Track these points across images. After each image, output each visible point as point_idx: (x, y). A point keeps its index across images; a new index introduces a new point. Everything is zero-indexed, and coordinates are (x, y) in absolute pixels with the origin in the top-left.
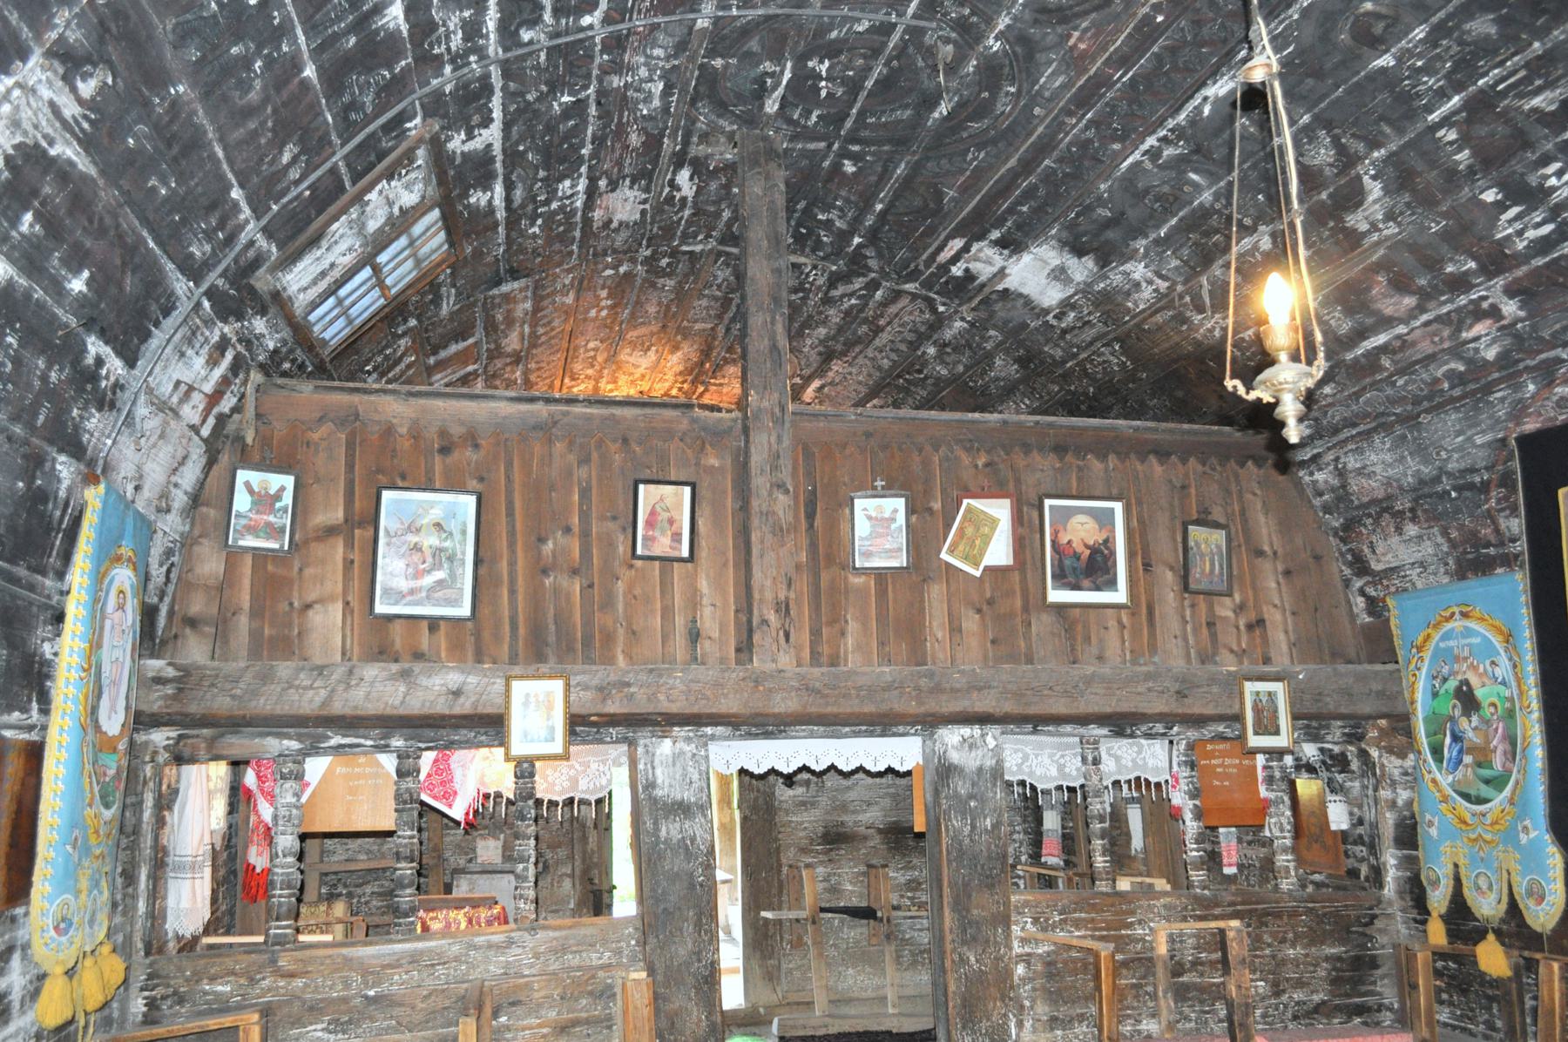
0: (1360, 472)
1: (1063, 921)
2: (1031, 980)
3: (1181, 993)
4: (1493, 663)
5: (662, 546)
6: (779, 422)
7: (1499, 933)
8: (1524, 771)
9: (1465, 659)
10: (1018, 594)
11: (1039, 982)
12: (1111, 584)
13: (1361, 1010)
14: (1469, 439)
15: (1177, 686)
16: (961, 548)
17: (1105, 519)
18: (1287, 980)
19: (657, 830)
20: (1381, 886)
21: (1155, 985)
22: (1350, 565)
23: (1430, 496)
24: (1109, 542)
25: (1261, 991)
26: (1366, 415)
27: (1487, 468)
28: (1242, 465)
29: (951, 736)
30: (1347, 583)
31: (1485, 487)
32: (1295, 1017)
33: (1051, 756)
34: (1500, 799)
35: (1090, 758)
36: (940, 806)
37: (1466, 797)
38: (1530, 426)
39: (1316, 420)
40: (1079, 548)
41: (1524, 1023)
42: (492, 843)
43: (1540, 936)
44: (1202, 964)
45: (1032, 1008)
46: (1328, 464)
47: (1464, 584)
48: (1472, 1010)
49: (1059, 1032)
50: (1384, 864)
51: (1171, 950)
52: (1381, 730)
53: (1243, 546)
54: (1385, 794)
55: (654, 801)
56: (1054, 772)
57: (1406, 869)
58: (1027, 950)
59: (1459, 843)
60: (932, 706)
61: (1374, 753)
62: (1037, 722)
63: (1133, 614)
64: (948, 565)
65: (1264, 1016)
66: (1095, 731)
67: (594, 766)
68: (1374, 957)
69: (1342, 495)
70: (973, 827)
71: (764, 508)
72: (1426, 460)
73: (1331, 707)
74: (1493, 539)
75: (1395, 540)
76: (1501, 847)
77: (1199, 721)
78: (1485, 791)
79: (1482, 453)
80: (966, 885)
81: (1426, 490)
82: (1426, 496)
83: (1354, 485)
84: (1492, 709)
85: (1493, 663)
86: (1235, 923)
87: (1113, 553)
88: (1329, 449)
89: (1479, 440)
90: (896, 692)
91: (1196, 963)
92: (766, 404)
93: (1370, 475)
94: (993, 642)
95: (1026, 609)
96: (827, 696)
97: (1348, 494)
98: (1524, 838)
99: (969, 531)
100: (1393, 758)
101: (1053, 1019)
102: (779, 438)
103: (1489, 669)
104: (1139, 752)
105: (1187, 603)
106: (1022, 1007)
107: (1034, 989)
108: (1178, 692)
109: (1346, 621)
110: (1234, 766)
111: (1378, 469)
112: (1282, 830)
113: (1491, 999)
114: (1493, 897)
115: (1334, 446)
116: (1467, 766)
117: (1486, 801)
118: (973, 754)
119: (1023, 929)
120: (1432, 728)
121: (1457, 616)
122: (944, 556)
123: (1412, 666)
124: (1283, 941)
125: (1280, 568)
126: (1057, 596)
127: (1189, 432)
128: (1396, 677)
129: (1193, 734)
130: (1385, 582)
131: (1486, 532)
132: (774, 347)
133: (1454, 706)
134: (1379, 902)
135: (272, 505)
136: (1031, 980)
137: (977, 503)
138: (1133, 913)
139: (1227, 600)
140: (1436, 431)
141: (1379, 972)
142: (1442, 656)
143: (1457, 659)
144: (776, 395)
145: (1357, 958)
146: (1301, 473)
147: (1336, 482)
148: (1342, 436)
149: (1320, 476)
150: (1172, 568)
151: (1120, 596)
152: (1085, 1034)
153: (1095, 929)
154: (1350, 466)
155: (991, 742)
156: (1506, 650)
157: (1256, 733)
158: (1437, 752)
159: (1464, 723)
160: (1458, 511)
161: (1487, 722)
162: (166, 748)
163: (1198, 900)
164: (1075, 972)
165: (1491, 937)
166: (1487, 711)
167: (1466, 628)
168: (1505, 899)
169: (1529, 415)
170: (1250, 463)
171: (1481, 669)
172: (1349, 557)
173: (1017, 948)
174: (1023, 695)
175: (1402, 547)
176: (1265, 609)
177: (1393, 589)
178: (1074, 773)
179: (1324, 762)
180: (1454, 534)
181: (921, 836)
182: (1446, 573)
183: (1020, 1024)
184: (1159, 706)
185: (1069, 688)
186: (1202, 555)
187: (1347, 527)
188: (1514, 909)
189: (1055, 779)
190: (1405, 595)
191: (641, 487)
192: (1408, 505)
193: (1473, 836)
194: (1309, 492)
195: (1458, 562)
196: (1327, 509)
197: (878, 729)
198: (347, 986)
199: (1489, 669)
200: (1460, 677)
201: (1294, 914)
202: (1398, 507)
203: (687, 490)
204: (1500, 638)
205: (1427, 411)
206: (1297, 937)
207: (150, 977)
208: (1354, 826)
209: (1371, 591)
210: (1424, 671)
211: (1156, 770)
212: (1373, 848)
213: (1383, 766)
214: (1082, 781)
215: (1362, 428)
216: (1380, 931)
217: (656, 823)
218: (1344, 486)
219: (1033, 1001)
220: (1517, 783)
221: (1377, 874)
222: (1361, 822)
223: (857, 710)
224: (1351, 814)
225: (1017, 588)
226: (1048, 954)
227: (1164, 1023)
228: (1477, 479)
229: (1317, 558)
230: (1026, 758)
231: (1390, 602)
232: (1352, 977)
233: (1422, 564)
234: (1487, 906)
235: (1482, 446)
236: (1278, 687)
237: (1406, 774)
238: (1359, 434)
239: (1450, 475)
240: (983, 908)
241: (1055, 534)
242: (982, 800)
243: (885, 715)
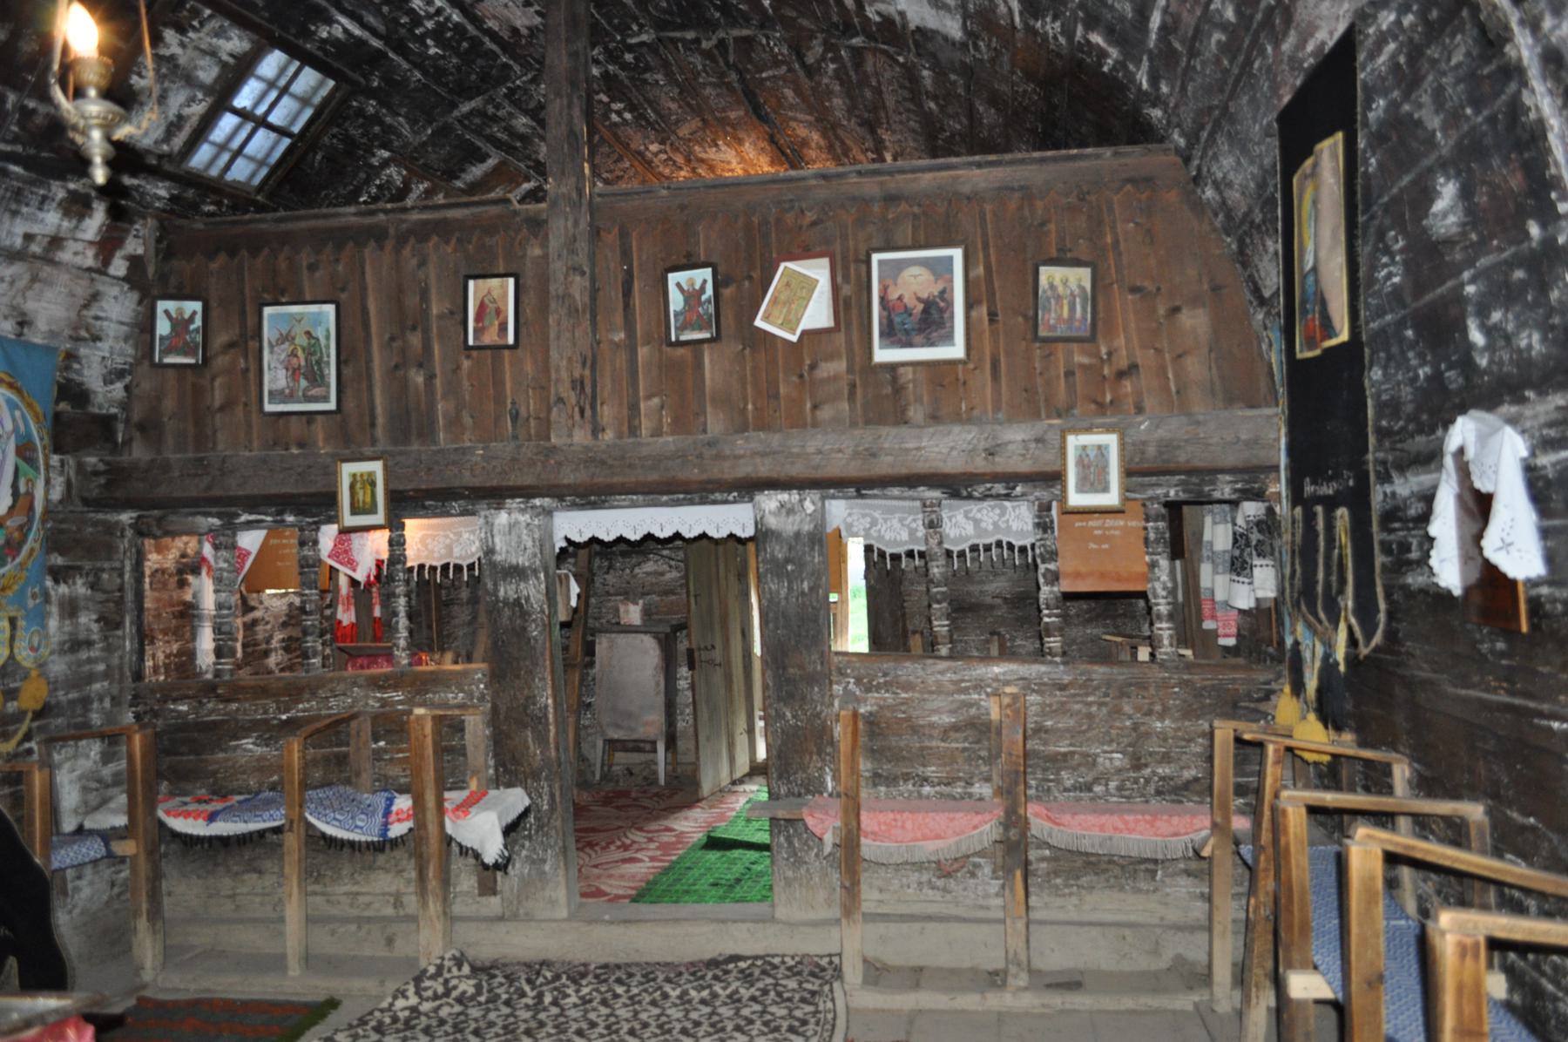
5: (490, 338)
6: (576, 206)
18: (1151, 754)
19: (496, 590)
24: (946, 294)
25: (1117, 763)
29: (770, 502)
32: (1159, 793)
33: (901, 520)
40: (909, 300)
42: (632, 608)
49: (883, 789)
55: (493, 565)
56: (905, 536)
65: (1120, 788)
67: (466, 536)
70: (790, 589)
71: (561, 292)
87: (950, 304)
92: (564, 190)
96: (611, 467)
102: (576, 223)
104: (1002, 514)
118: (791, 519)
124: (1149, 713)
132: (572, 134)
135: (187, 327)
137: (791, 265)
144: (573, 179)
152: (911, 792)
155: (809, 507)
162: (131, 526)
186: (1059, 298)
189: (906, 543)
191: (471, 283)
197: (696, 497)
198: (266, 712)
203: (511, 281)
207: (135, 697)
211: (1021, 533)
217: (495, 585)
223: (641, 478)
226: (871, 713)
230: (874, 523)
242: (801, 565)
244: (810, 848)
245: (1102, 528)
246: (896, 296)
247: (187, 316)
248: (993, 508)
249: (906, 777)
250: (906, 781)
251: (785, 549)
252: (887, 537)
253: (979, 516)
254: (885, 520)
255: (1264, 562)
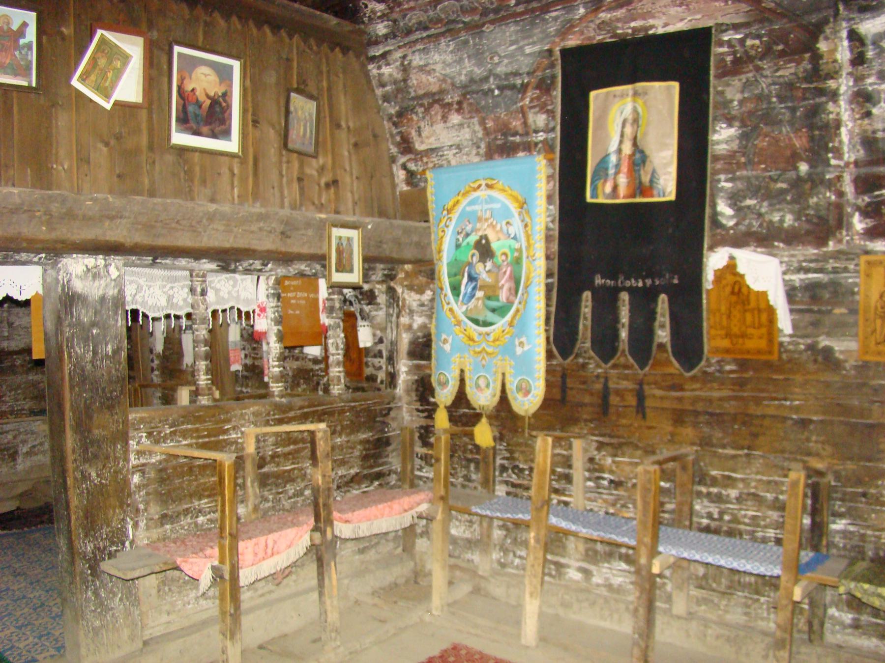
0: (421, 69)
1: (173, 433)
2: (145, 486)
3: (264, 481)
4: (508, 223)
7: (489, 417)
8: (525, 302)
9: (486, 220)
10: (145, 132)
11: (151, 488)
12: (226, 134)
13: (379, 476)
14: (521, 49)
15: (281, 228)
16: (93, 77)
17: (224, 74)
20: (395, 387)
21: (244, 477)
22: (398, 145)
23: (477, 93)
24: (226, 95)
26: (439, 21)
27: (528, 74)
28: (332, 50)
29: (76, 267)
30: (393, 160)
31: (524, 87)
34: (501, 323)
35: (199, 290)
36: (62, 333)
37: (476, 322)
38: (573, 42)
39: (395, 21)
40: (202, 97)
41: (494, 476)
43: (523, 418)
44: (278, 456)
45: (146, 510)
46: (396, 61)
47: (491, 163)
48: (454, 469)
50: (398, 371)
51: (258, 448)
52: (407, 273)
53: (328, 119)
54: (404, 320)
56: (163, 302)
57: (415, 374)
58: (143, 461)
59: (467, 355)
60: (64, 232)
61: (399, 290)
62: (157, 254)
63: (242, 163)
64: (80, 95)
66: (207, 265)
68: (388, 438)
69: (402, 87)
70: (95, 353)
72: (480, 64)
73: (387, 253)
74: (520, 130)
75: (439, 127)
76: (500, 357)
77: (286, 259)
78: (490, 317)
79: (530, 60)
80: (87, 408)
81: (474, 87)
82: (473, 92)
83: (413, 81)
84: (504, 258)
85: (508, 223)
86: (323, 426)
87: (229, 107)
88: (400, 47)
89: (528, 50)
90: (25, 216)
91: (274, 456)
93: (429, 73)
94: (119, 176)
95: (151, 148)
97: (407, 87)
98: (519, 351)
99: (102, 62)
100: (413, 294)
101: (164, 516)
103: (505, 228)
104: (234, 286)
105: (284, 159)
106: (138, 510)
107: (148, 494)
108: (283, 233)
109: (389, 190)
110: (304, 298)
111: (438, 67)
112: (337, 349)
113: (469, 461)
114: (488, 393)
115: (405, 45)
116: (478, 299)
117: (491, 324)
118: (97, 283)
119: (138, 443)
120: (454, 271)
121: (483, 187)
122: (75, 83)
123: (442, 224)
125: (352, 141)
126: (180, 138)
127: (297, 11)
128: (427, 232)
129: (281, 271)
130: (425, 160)
131: (516, 124)
133: (473, 256)
134: (394, 398)
135: (17, 41)
136: (145, 486)
137: (110, 36)
138: (228, 421)
139: (314, 161)
140: (495, 39)
141: (390, 448)
142: (467, 217)
143: (479, 219)
145: (379, 440)
146: (370, 67)
147: (399, 76)
148: (413, 37)
149: (386, 70)
150: (273, 127)
151: (232, 145)
152: (190, 524)
153: (199, 437)
154: (414, 63)
155: (114, 273)
156: (520, 214)
157: (337, 271)
158: (456, 289)
159: (480, 267)
160: (496, 106)
161: (499, 267)
163: (279, 408)
164: (182, 475)
165: (484, 420)
166: (499, 259)
167: (489, 196)
168: (498, 394)
169: (574, 33)
170: (337, 49)
171: (498, 228)
172: (398, 139)
173: (133, 460)
174: (152, 227)
175: (445, 132)
176: (338, 172)
177: (431, 165)
178: (181, 303)
179: (356, 297)
180: (490, 124)
181: (40, 363)
182: (478, 154)
183: (136, 525)
184: (267, 244)
185: (194, 223)
186: (299, 120)
187: (400, 114)
188: (504, 399)
189: (165, 308)
190: (442, 170)
192: (456, 99)
193: (478, 350)
194: (374, 83)
195: (489, 146)
196: (386, 98)
199: (505, 228)
200: (480, 233)
201: (342, 412)
202: (448, 99)
204: (516, 205)
205: (492, 22)
206: (343, 428)
208: (376, 344)
209: (412, 166)
210: (451, 228)
212: (391, 360)
213: (404, 299)
214: (190, 310)
215: (433, 31)
216: (393, 419)
218: (405, 80)
219: (147, 503)
220: (518, 311)
221: (392, 378)
222: (381, 341)
224: (374, 335)
225: (144, 126)
226: (160, 462)
227: (251, 507)
228: (519, 82)
229: (375, 136)
230: (139, 289)
231: (429, 175)
232: (375, 454)
233: (459, 147)
234: (483, 398)
235: (530, 55)
236: (354, 234)
237: (422, 305)
238: (429, 36)
239: (497, 76)
240: (104, 428)
241: (181, 80)
242: (104, 328)
243: (11, 240)
244: (115, 595)
245: (295, 298)
246: (190, 89)
247: (15, 27)
248: (228, 279)
249: (187, 512)
250: (185, 515)
251: (91, 313)
252: (150, 303)
253: (218, 286)
254: (149, 287)
255: (366, 323)
